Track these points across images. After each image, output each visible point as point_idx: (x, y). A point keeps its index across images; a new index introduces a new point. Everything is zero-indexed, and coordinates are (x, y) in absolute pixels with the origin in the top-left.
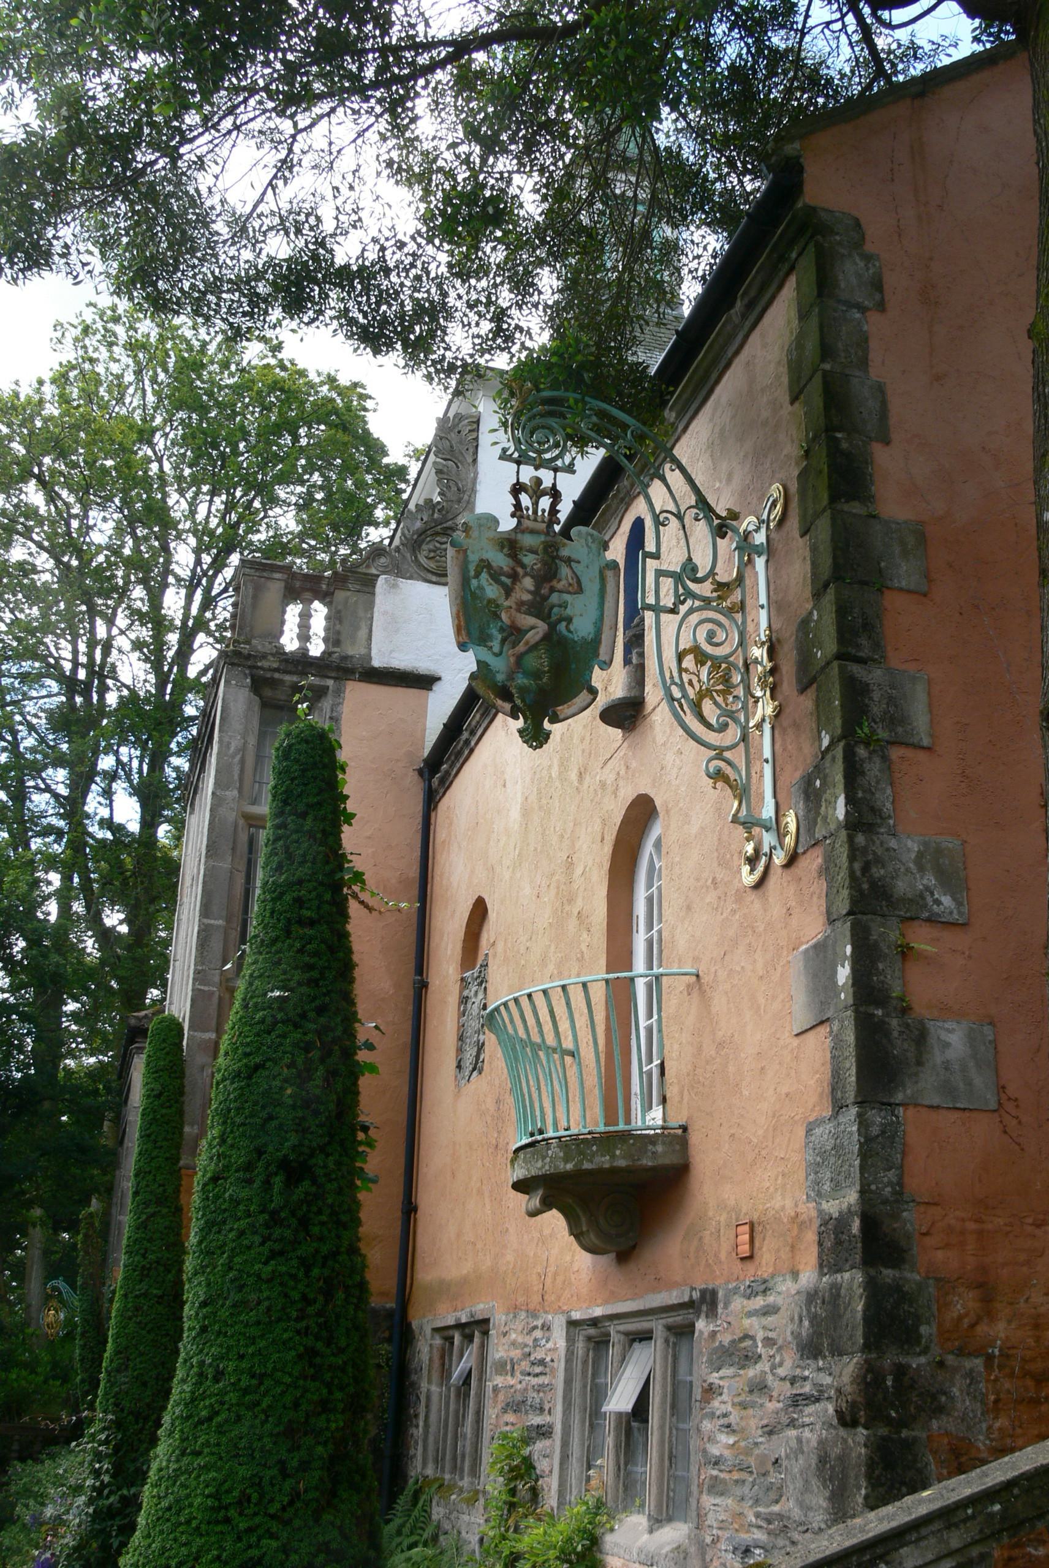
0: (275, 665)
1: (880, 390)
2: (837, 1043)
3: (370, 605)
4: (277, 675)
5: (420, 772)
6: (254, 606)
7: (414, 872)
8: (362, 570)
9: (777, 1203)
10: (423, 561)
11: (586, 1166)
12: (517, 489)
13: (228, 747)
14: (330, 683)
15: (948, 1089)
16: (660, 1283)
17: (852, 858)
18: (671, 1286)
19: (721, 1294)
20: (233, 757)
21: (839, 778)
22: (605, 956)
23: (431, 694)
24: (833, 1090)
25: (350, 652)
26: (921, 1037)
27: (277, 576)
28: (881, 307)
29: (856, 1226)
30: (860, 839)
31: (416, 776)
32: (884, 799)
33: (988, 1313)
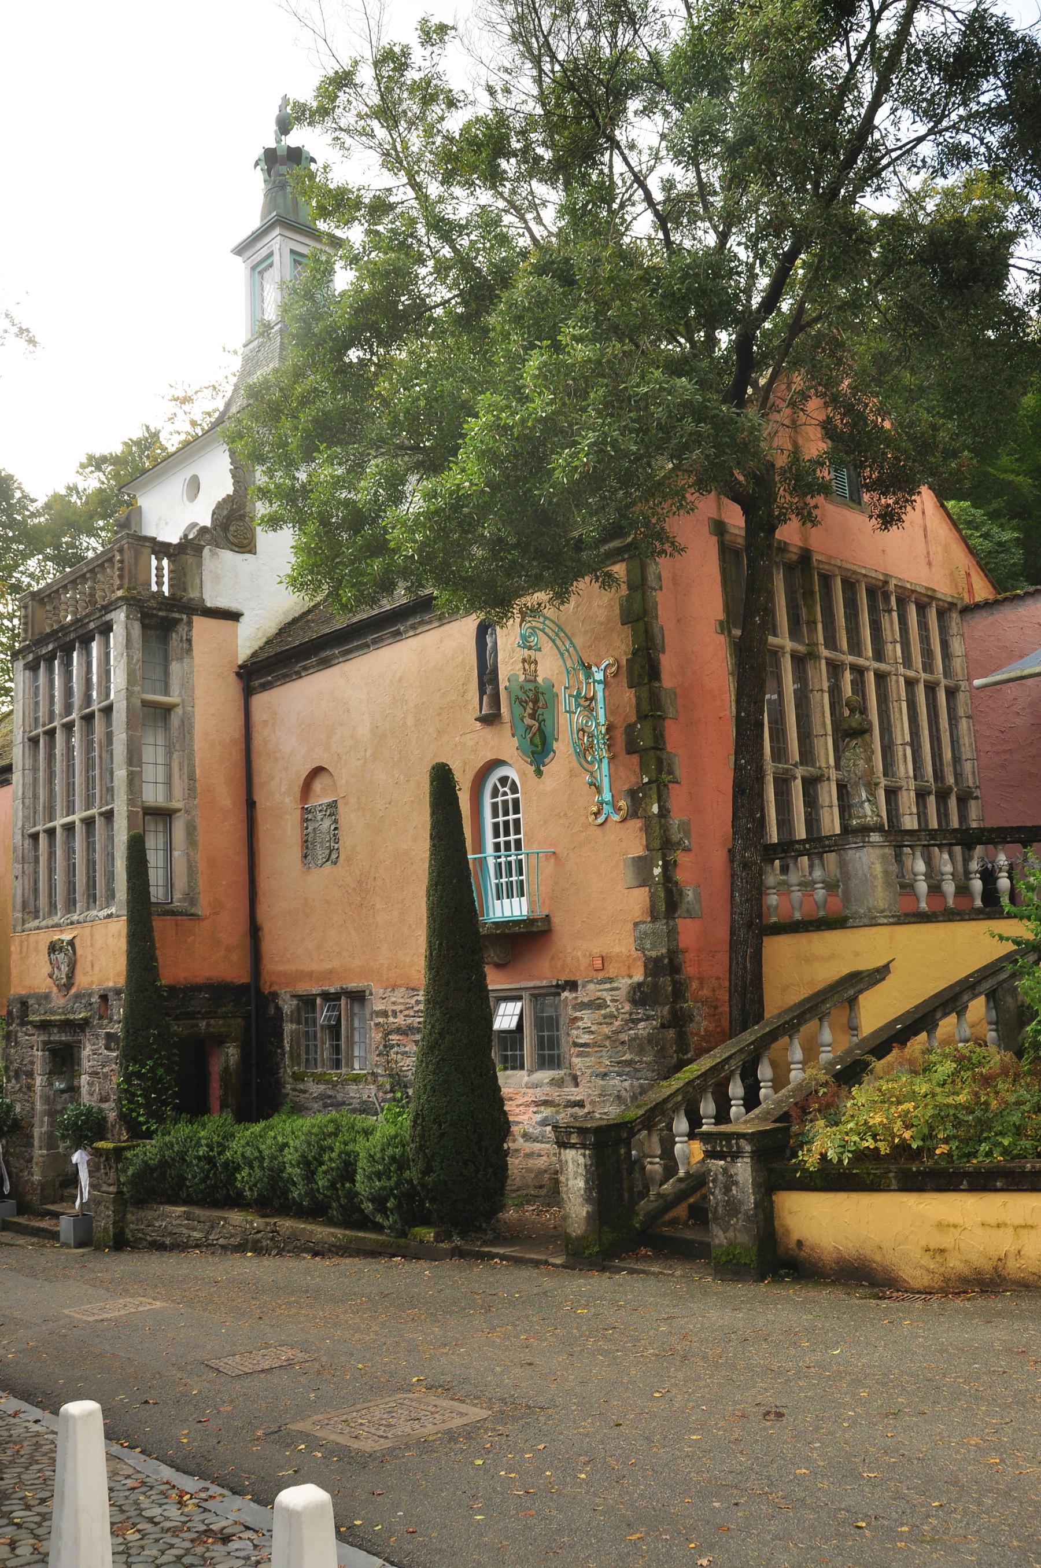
0: (155, 605)
1: (662, 628)
2: (653, 896)
3: (200, 565)
4: (155, 612)
5: (238, 674)
6: (136, 564)
7: (238, 733)
8: (196, 542)
9: (617, 949)
10: (231, 538)
11: (507, 931)
12: (524, 661)
13: (132, 659)
14: (185, 617)
15: (688, 911)
16: (532, 978)
17: (660, 829)
18: (541, 979)
19: (579, 982)
20: (136, 664)
21: (655, 796)
22: (427, 810)
23: (239, 625)
24: (651, 912)
25: (192, 596)
26: (681, 894)
27: (147, 544)
28: (661, 588)
29: (666, 961)
30: (663, 820)
31: (233, 678)
32: (669, 806)
33: (702, 988)
